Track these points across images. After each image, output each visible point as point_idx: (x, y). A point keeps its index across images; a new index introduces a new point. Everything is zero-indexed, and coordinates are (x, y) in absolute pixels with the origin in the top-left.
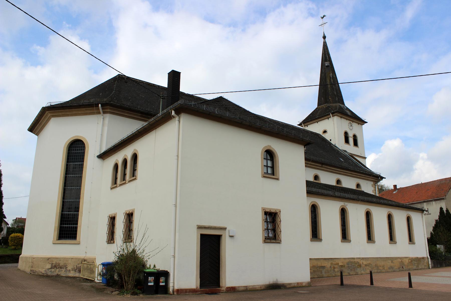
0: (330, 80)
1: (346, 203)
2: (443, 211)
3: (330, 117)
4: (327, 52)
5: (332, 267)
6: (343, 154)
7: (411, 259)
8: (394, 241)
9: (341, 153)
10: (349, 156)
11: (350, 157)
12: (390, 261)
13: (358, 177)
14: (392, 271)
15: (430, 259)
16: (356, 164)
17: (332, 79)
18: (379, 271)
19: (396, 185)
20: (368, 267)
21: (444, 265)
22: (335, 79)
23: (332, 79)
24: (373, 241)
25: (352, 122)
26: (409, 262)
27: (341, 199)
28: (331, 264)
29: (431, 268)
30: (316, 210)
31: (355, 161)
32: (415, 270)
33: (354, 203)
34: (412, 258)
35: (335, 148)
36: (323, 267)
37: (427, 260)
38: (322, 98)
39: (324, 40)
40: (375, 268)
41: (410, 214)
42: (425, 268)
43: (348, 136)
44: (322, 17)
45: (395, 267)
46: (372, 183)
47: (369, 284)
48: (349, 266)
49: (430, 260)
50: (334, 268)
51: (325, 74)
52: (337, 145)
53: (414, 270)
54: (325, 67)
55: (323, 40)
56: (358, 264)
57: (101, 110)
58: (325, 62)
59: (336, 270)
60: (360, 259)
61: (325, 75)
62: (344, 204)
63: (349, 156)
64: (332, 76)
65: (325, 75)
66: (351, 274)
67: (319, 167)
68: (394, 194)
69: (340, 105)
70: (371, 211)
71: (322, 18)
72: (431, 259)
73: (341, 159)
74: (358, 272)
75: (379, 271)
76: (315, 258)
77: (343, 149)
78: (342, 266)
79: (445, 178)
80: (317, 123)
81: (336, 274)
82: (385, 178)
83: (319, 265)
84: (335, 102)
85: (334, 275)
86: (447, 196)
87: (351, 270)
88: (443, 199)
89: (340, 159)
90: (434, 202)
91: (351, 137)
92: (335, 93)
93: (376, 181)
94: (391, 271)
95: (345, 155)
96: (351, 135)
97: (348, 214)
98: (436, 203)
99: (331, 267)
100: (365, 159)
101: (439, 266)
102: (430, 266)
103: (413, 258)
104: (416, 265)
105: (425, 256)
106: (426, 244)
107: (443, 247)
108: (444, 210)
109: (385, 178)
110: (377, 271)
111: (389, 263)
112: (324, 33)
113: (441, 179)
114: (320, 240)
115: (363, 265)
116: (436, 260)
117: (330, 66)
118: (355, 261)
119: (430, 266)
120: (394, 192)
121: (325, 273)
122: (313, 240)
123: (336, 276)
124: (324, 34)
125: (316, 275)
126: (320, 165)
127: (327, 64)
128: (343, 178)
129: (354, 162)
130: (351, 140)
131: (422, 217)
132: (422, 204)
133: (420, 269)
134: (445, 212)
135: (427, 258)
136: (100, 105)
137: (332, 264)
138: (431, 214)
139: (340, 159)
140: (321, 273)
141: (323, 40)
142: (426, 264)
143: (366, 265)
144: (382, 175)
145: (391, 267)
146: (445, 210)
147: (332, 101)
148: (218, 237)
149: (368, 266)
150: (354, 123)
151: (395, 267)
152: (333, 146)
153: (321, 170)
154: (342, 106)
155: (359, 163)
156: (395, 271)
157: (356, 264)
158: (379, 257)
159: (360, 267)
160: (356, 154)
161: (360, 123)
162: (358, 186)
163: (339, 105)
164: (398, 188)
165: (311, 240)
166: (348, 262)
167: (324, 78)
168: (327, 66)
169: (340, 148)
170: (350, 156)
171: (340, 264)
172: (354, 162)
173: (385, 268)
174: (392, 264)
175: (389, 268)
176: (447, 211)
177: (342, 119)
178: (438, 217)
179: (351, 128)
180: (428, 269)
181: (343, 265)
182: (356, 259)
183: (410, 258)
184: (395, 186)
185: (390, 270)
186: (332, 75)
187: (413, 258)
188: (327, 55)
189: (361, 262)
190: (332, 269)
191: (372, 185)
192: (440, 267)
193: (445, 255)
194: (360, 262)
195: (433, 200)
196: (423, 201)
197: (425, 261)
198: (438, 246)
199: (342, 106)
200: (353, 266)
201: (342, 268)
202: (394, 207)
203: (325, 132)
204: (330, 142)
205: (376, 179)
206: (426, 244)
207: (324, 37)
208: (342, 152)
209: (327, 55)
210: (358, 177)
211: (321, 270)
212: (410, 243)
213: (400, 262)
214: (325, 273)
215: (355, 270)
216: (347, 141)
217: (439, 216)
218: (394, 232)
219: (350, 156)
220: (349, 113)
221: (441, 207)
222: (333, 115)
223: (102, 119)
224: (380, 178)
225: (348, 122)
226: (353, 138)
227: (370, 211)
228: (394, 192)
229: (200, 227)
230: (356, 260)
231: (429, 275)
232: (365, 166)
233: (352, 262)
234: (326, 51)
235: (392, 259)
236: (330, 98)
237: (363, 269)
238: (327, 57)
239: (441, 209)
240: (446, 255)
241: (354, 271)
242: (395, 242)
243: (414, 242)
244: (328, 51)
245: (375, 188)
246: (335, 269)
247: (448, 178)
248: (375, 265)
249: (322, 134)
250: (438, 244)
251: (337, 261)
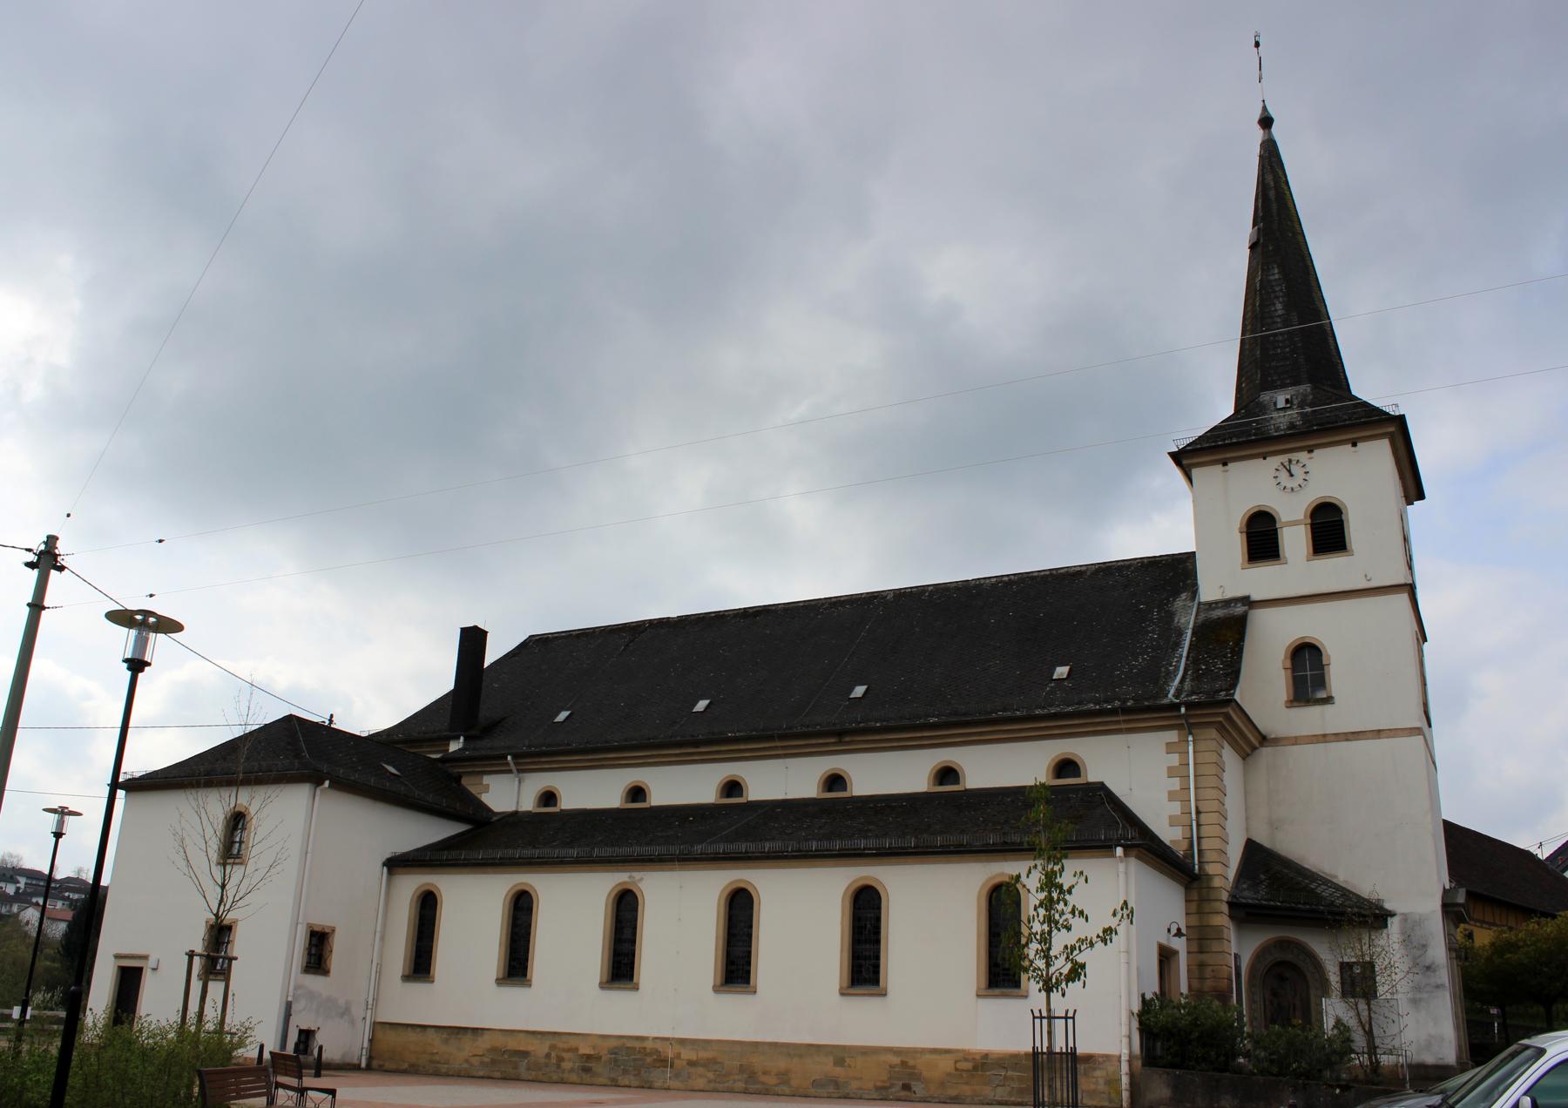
1: (637, 875)
5: (553, 1055)
7: (978, 1057)
12: (831, 1059)
18: (758, 1086)
26: (956, 1069)
34: (986, 1056)
40: (736, 1077)
56: (655, 1057)
57: (512, 767)
59: (566, 1065)
74: (651, 1079)
78: (589, 1057)
83: (509, 1048)
87: (625, 1072)
89: (386, 766)
99: (548, 1056)
110: (746, 1088)
111: (826, 1067)
114: (326, 972)
118: (645, 1048)
121: (528, 1069)
124: (1265, 108)
125: (498, 1071)
126: (832, 740)
128: (849, 764)
136: (509, 758)
137: (553, 1047)
139: (386, 766)
140: (516, 1068)
141: (1260, 132)
143: (691, 1063)
148: (139, 970)
153: (1012, 742)
157: (650, 1054)
160: (1331, 591)
161: (1228, 455)
181: (592, 1053)
189: (670, 1053)
190: (554, 1061)
207: (1266, 122)
211: (514, 1059)
214: (528, 1069)
215: (639, 1073)
223: (517, 783)
229: (117, 957)
230: (649, 1045)
233: (634, 1048)
235: (841, 1054)
241: (635, 1075)
246: (563, 1064)
248: (741, 1065)
251: (573, 1042)
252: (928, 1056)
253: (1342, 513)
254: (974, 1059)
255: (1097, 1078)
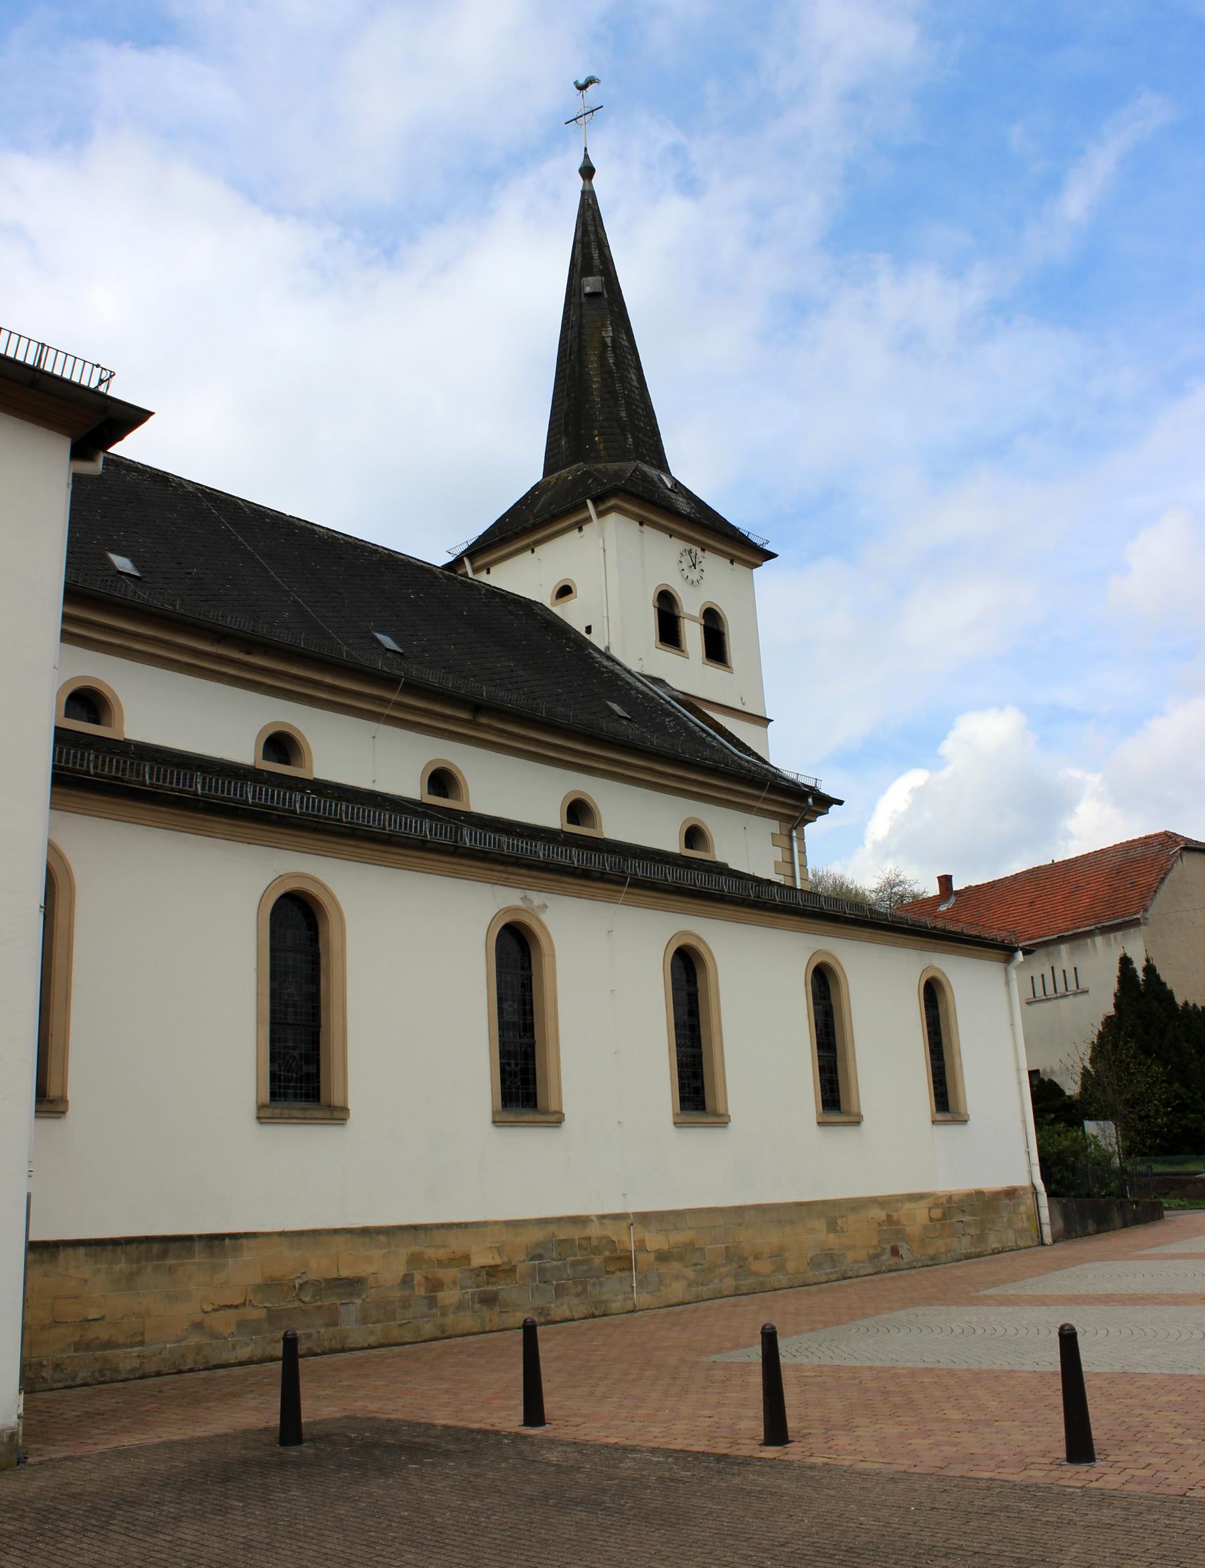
0: (603, 358)
1: (537, 898)
2: (1134, 970)
3: (588, 520)
4: (596, 233)
5: (418, 1277)
6: (639, 691)
7: (944, 1200)
8: (849, 1113)
9: (628, 683)
10: (669, 699)
11: (673, 707)
12: (820, 1224)
13: (695, 789)
14: (833, 1277)
15: (1045, 1194)
16: (701, 737)
17: (610, 354)
18: (750, 1280)
19: (951, 876)
20: (675, 1266)
21: (1117, 1219)
22: (624, 351)
23: (610, 354)
24: (715, 1113)
25: (699, 550)
26: (931, 1220)
27: (499, 868)
28: (408, 1262)
29: (1048, 1239)
30: (320, 930)
31: (697, 725)
32: (968, 1257)
33: (592, 897)
34: (950, 1198)
35: (606, 663)
36: (352, 1285)
37: (1029, 1201)
38: (560, 439)
39: (584, 184)
40: (723, 1270)
41: (943, 969)
42: (1021, 1243)
43: (676, 613)
44: (582, 82)
45: (850, 1255)
46: (774, 826)
47: (510, 1417)
48: (542, 1270)
49: (1043, 1199)
50: (435, 1285)
51: (581, 327)
52: (615, 653)
53: (958, 1260)
54: (584, 300)
55: (579, 182)
56: (607, 1253)
58: (582, 277)
59: (449, 1296)
60: (625, 1224)
61: (580, 334)
62: (524, 899)
63: (669, 703)
64: (613, 340)
65: (580, 334)
66: (558, 1319)
67: (461, 726)
68: (943, 913)
69: (646, 468)
70: (705, 944)
71: (582, 88)
72: (1050, 1194)
73: (615, 707)
74: (605, 1298)
75: (750, 1280)
76: (287, 1229)
77: (646, 673)
78: (492, 1271)
79: (1146, 838)
80: (533, 551)
81: (449, 1320)
82: (840, 803)
83: (312, 1276)
84: (623, 456)
85: (428, 1329)
86: (1151, 911)
87: (560, 1291)
88: (1136, 923)
89: (610, 703)
90: (1099, 940)
91: (693, 619)
92: (623, 414)
93: (795, 818)
94: (824, 1278)
95: (651, 694)
96: (690, 607)
97: (546, 962)
98: (1109, 944)
99: (407, 1281)
100: (766, 727)
101: (1091, 1227)
102: (1047, 1230)
103: (954, 1198)
104: (972, 1231)
105: (1021, 1181)
106: (1024, 1122)
107: (1116, 1129)
108: (1137, 970)
109: (840, 803)
110: (737, 1287)
111: (817, 1236)
112: (589, 152)
113: (1127, 842)
115: (642, 1256)
116: (1075, 1196)
117: (606, 296)
118: (589, 1238)
119: (1047, 1230)
120: (943, 908)
121: (364, 1320)
122: (277, 1111)
123: (449, 1337)
124: (586, 156)
126: (465, 715)
127: (591, 284)
128: (603, 794)
129: (687, 728)
130: (693, 634)
131: (1007, 983)
132: (1051, 949)
133: (993, 1250)
134: (1141, 975)
135: (1030, 1191)
137: (415, 1260)
138: (1087, 992)
139: (610, 703)
140: (334, 1323)
142: (1026, 1224)
144: (825, 789)
145: (830, 1257)
146: (1139, 965)
147: (605, 448)
149: (680, 1258)
150: (710, 553)
151: (850, 1255)
152: (596, 655)
154: (653, 472)
155: (714, 733)
156: (850, 1274)
157: (597, 1250)
158: (750, 1201)
159: (620, 1270)
162: (694, 835)
163: (636, 469)
164: (957, 886)
165: (264, 1116)
166: (539, 1244)
167: (576, 346)
168: (588, 295)
169: (634, 667)
170: (673, 702)
171: (481, 1258)
172: (692, 725)
173: (791, 1266)
174: (832, 1236)
175: (815, 1263)
176: (1150, 969)
177: (645, 528)
178: (1113, 1001)
179: (694, 575)
180: (1032, 1249)
181: (498, 1261)
182: (596, 1222)
183: (940, 1197)
184: (945, 881)
185: (820, 1275)
186: (611, 334)
187: (954, 1198)
188: (593, 245)
190: (421, 1291)
191: (772, 834)
192: (1098, 1232)
193: (1123, 1169)
194: (625, 1238)
195: (1097, 928)
196: (1055, 936)
197: (1022, 1209)
198: (1091, 1127)
199: (653, 472)
200: (574, 1264)
201: (493, 1284)
202: (847, 929)
203: (565, 591)
204: (587, 636)
205: (794, 807)
206: (1024, 1122)
207: (587, 172)
208: (639, 684)
209: (593, 245)
210: (695, 789)
211: (327, 1302)
212: (939, 1117)
213: (880, 1224)
215: (584, 1290)
216: (669, 633)
217: (1115, 995)
218: (845, 1061)
219: (673, 700)
220: (683, 505)
221: (1125, 954)
222: (602, 507)
224: (810, 800)
225: (678, 545)
226: (703, 622)
227: (702, 949)
228: (943, 908)
230: (594, 1231)
231: (1011, 1290)
232: (766, 763)
233: (572, 1241)
234: (591, 228)
236: (596, 439)
237: (641, 1283)
238: (596, 255)
239: (1125, 962)
240: (1129, 1169)
241: (578, 1295)
242: (853, 1119)
243: (962, 1110)
244: (599, 230)
245: (791, 849)
247: (1156, 835)
249: (553, 605)
250: (1090, 1119)
252: (909, 1206)
253: (1114, 1004)
254: (942, 1203)
255: (1020, 1214)
